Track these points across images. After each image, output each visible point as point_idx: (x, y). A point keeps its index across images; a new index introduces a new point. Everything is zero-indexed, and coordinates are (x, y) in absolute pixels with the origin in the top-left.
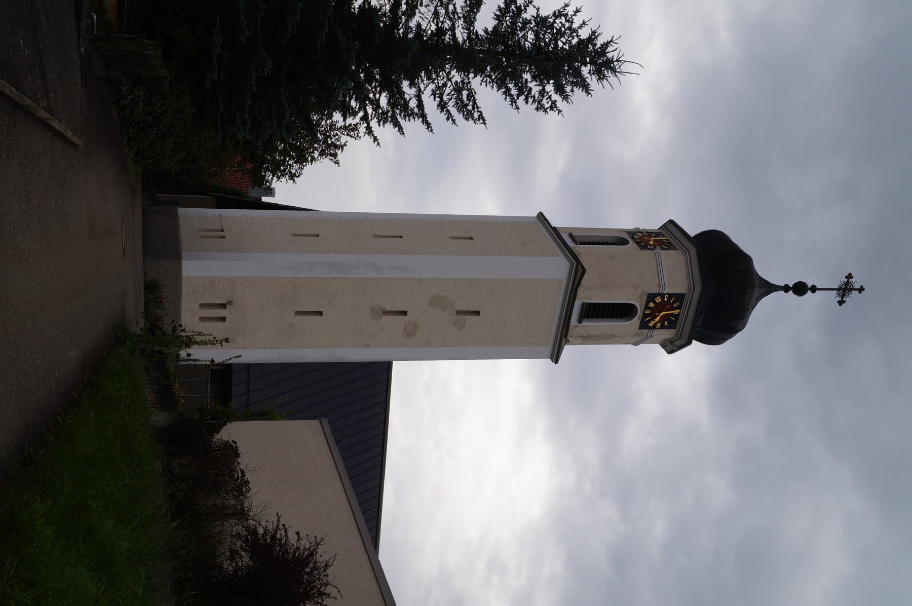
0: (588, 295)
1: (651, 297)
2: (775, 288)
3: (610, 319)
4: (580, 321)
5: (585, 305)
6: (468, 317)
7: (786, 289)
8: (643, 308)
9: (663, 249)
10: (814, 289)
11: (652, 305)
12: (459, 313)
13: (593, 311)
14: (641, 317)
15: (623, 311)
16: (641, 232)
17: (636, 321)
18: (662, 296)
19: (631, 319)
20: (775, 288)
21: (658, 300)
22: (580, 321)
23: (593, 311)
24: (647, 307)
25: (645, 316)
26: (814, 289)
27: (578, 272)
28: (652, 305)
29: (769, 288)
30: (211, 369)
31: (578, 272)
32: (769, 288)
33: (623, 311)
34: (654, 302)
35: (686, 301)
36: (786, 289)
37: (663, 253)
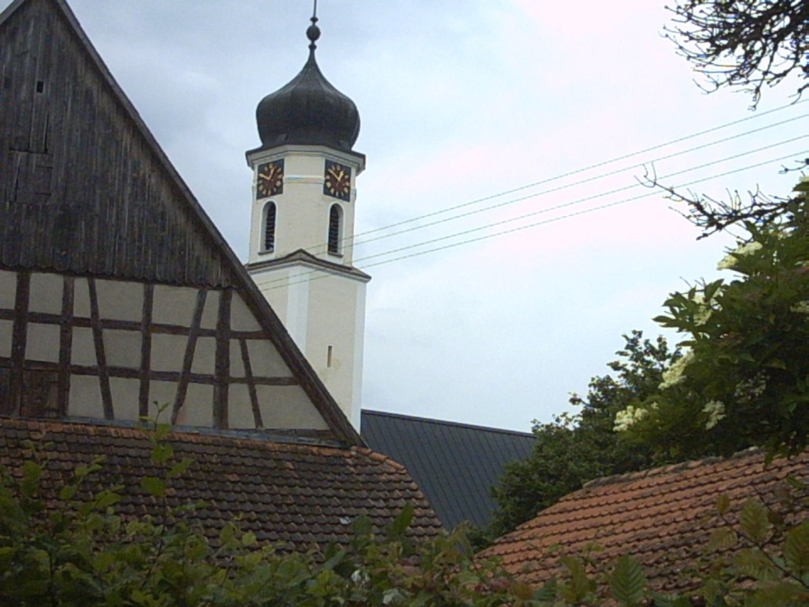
0: (319, 247)
1: (327, 191)
2: (312, 58)
3: (339, 228)
4: (340, 256)
5: (331, 252)
6: (333, 357)
7: (312, 48)
8: (334, 199)
9: (282, 172)
10: (314, 20)
11: (332, 191)
12: (329, 364)
13: (333, 246)
14: (341, 200)
15: (335, 213)
16: (258, 186)
17: (343, 204)
18: (326, 181)
19: (341, 210)
20: (312, 58)
21: (329, 185)
22: (340, 256)
23: (333, 246)
24: (334, 195)
25: (340, 197)
26: (314, 20)
27: (301, 257)
28: (332, 191)
29: (311, 65)
30: (268, 176)
31: (301, 257)
32: (311, 65)
33: (335, 213)
34: (330, 188)
35: (331, 158)
36: (312, 48)
37: (286, 176)
